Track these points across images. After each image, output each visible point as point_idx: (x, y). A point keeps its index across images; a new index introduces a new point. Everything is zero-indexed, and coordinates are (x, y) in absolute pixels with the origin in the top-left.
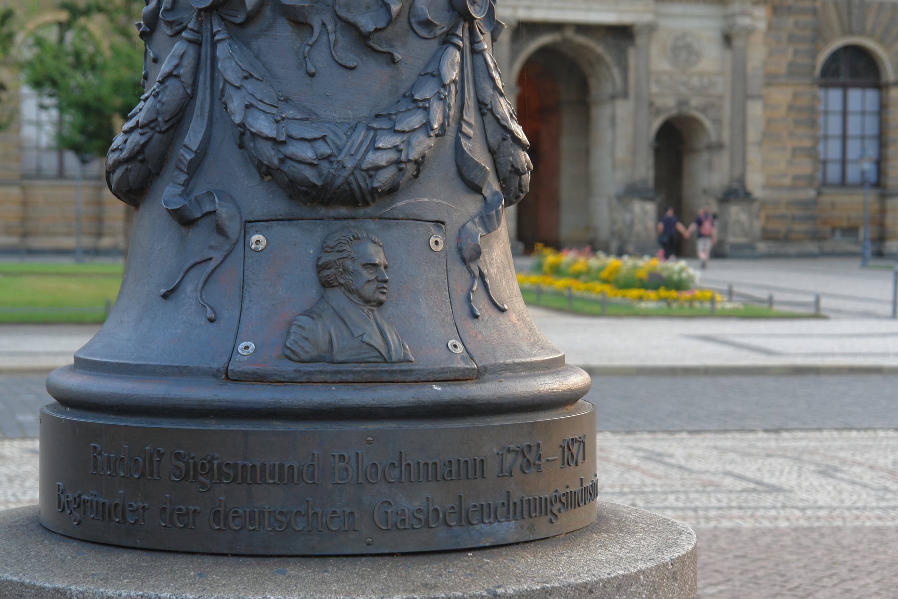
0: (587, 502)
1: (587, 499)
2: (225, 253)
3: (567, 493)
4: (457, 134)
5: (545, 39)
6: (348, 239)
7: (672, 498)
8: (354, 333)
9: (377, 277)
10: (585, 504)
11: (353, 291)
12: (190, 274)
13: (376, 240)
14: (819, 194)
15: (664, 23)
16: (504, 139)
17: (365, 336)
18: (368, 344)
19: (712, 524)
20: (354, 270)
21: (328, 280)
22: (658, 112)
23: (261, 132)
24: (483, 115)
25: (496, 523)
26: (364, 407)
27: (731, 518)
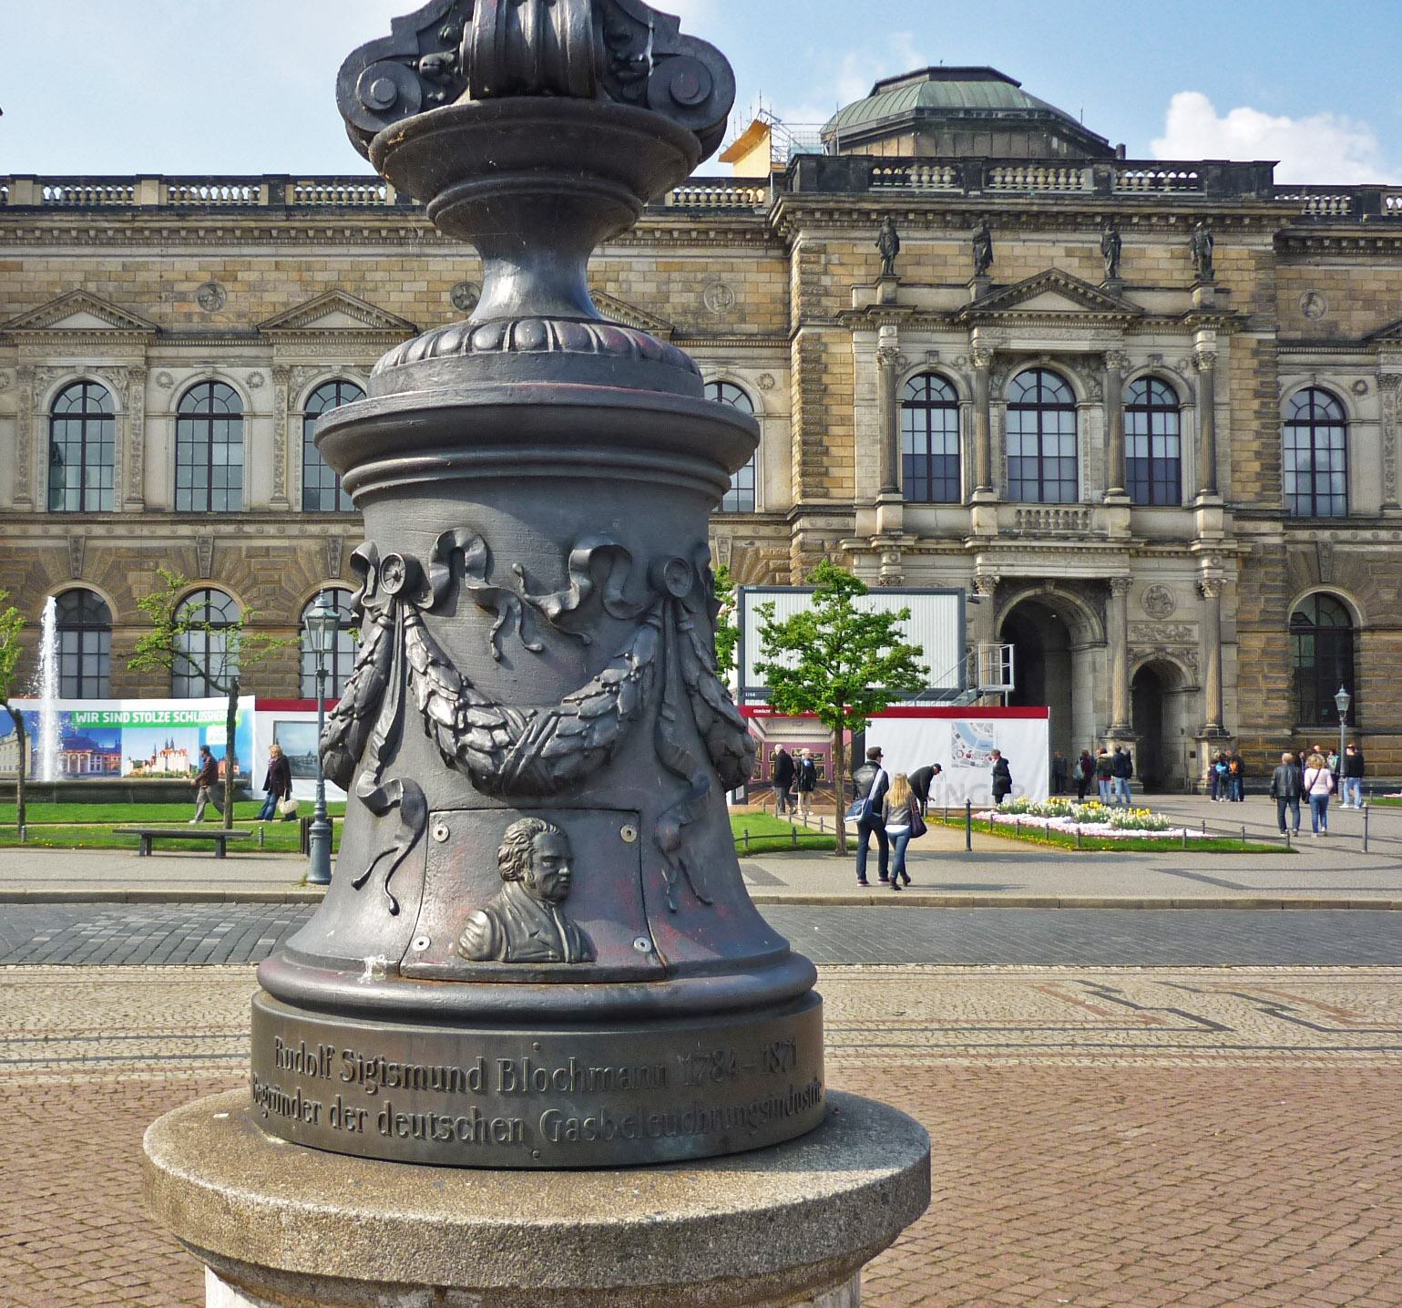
5: (1028, 593)
7: (1112, 1034)
14: (1295, 733)
15: (1139, 576)
19: (1149, 1063)
22: (1137, 657)
24: (690, 696)
27: (1169, 1056)
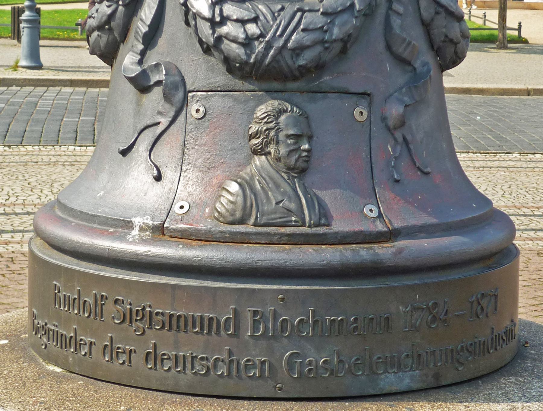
0: (498, 348)
1: (499, 345)
2: (170, 119)
3: (475, 343)
4: (387, 12)
10: (496, 350)
12: (142, 135)
16: (437, 13)
23: (201, 13)
25: (401, 373)
26: (278, 268)
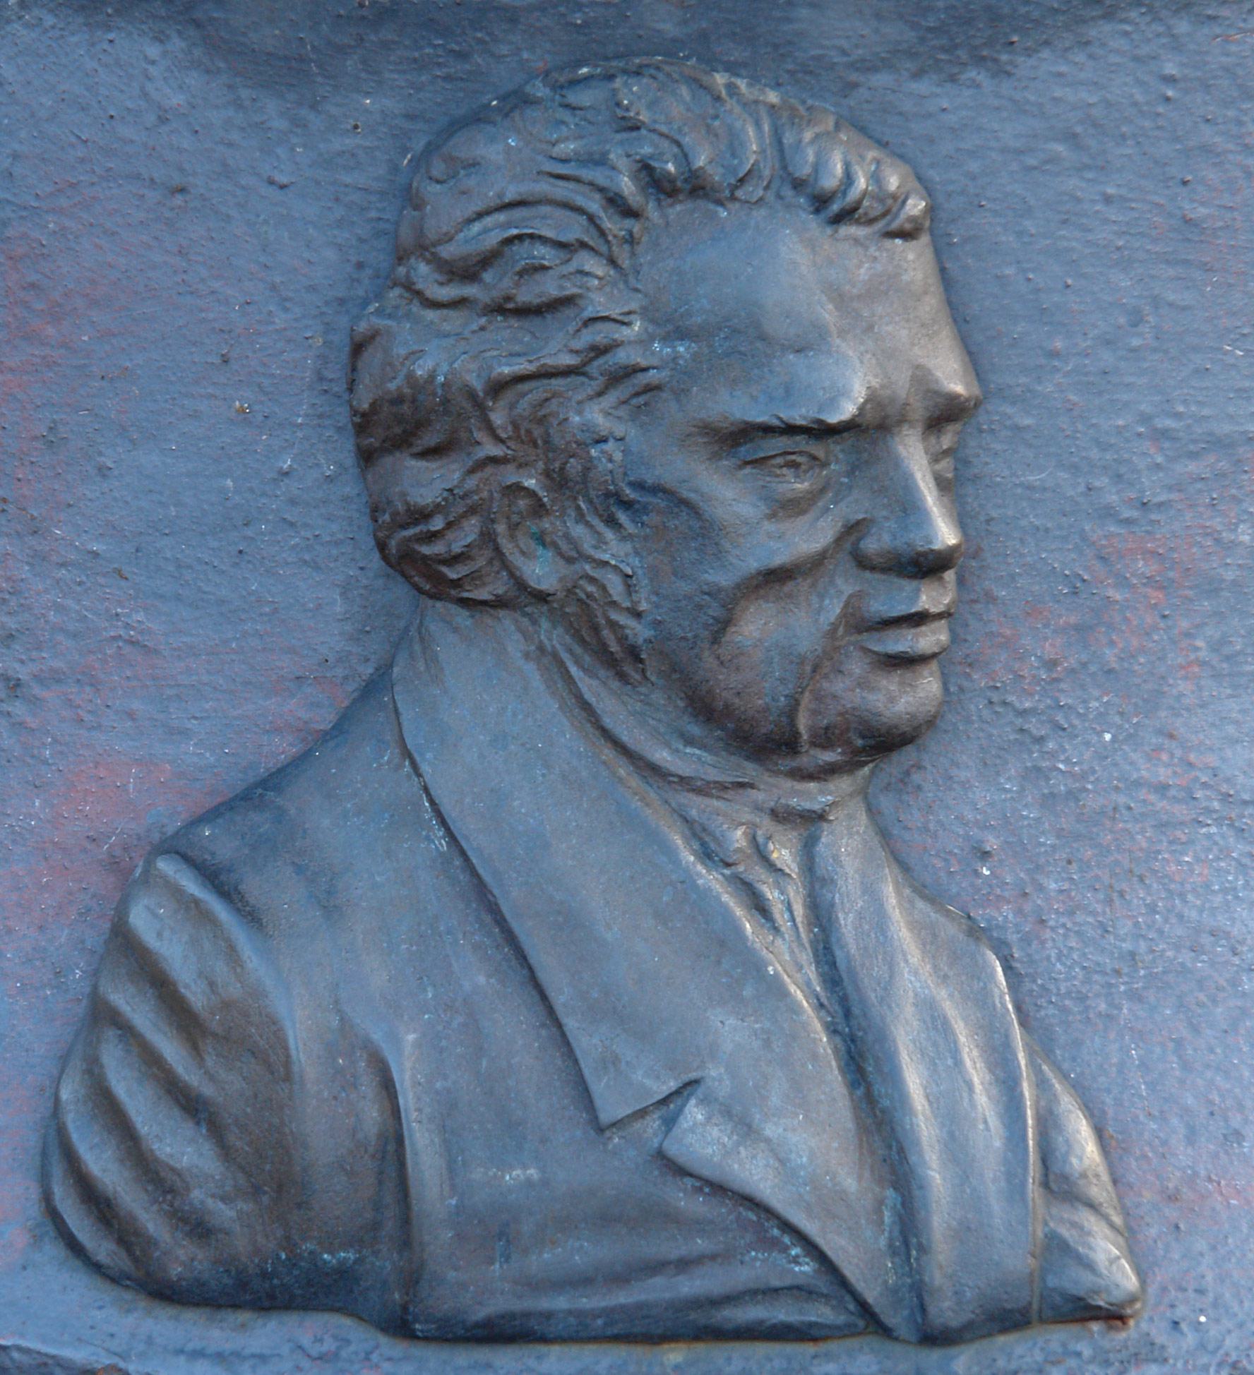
6: (594, 205)
8: (599, 1087)
9: (853, 530)
11: (634, 653)
13: (861, 183)
17: (694, 1113)
18: (718, 1189)
20: (639, 486)
21: (426, 550)
